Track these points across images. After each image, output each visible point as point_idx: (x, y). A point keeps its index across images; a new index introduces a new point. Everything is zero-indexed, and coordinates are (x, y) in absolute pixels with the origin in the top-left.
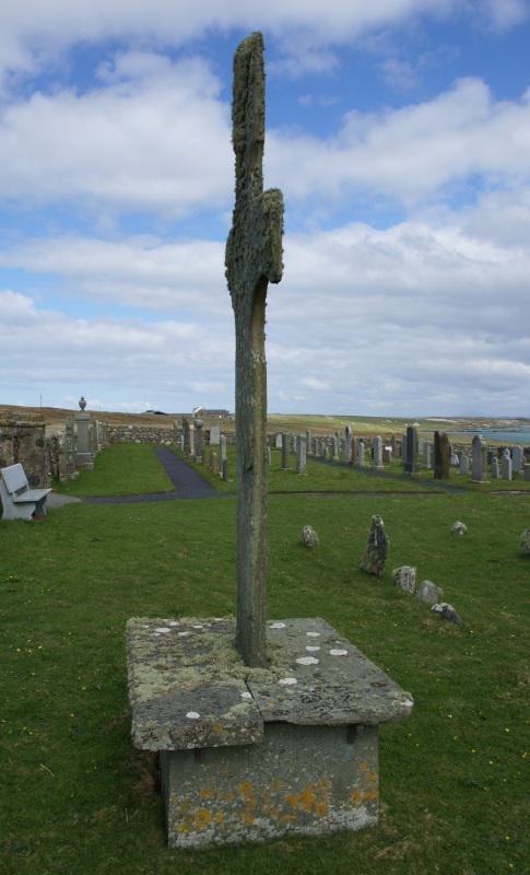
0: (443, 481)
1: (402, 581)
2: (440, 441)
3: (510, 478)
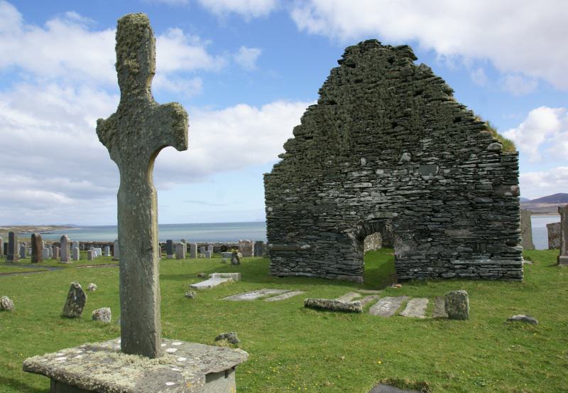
0: (39, 263)
1: (101, 316)
2: (35, 241)
3: (78, 259)
